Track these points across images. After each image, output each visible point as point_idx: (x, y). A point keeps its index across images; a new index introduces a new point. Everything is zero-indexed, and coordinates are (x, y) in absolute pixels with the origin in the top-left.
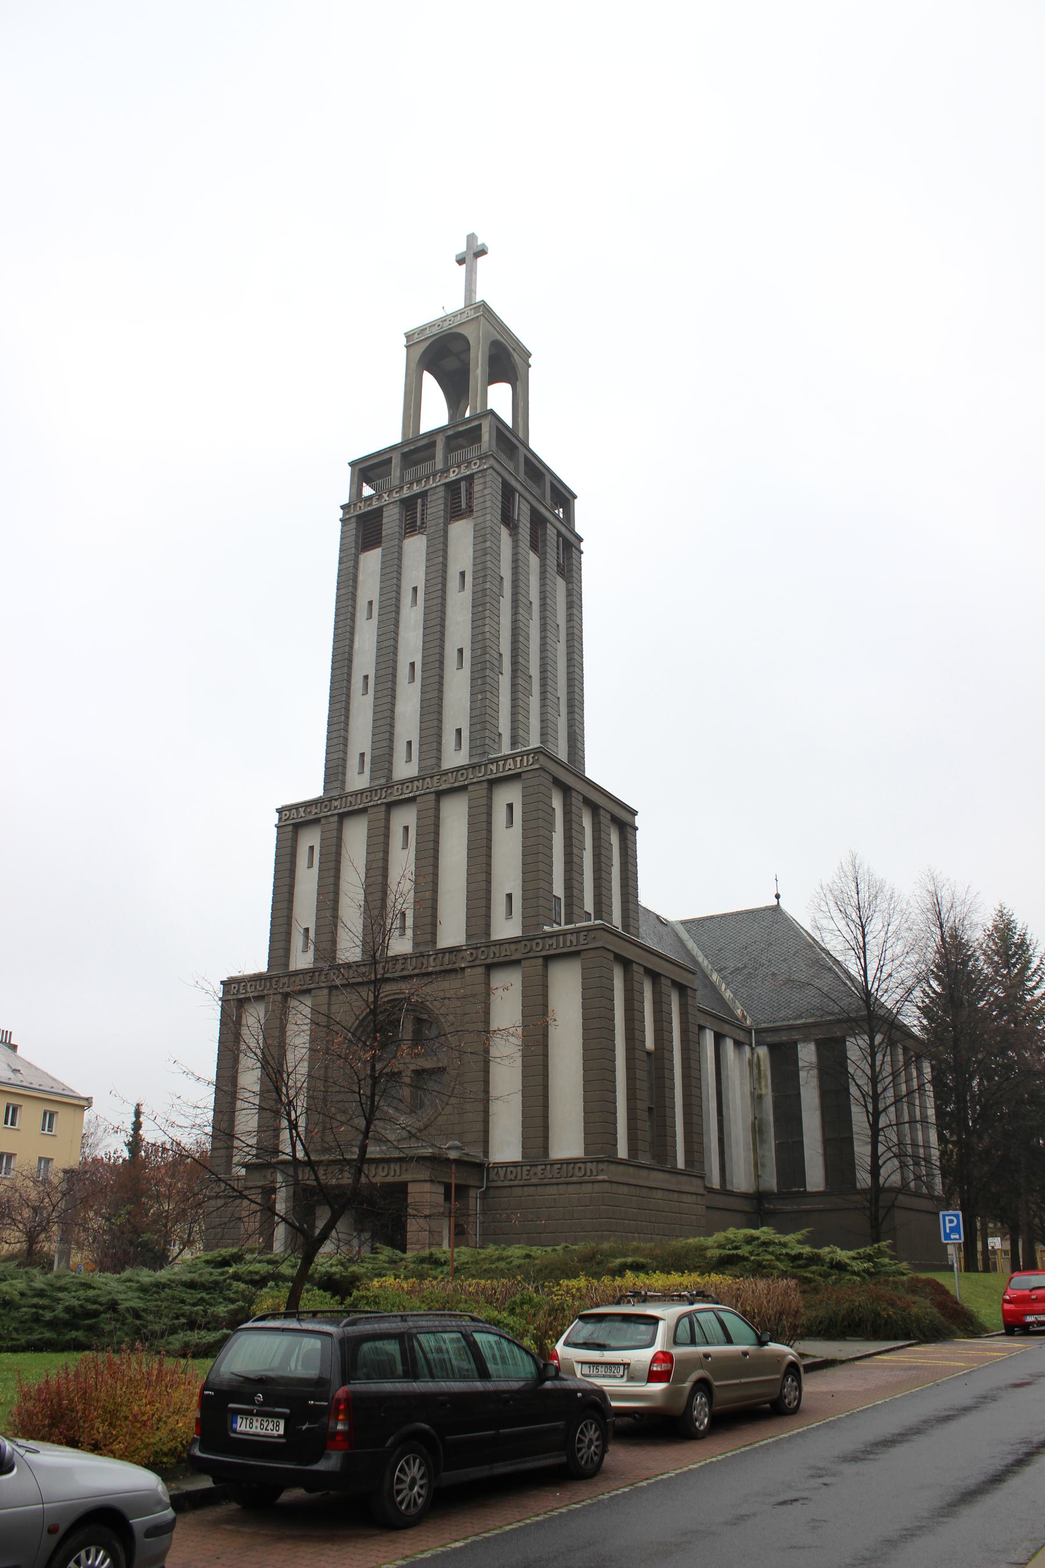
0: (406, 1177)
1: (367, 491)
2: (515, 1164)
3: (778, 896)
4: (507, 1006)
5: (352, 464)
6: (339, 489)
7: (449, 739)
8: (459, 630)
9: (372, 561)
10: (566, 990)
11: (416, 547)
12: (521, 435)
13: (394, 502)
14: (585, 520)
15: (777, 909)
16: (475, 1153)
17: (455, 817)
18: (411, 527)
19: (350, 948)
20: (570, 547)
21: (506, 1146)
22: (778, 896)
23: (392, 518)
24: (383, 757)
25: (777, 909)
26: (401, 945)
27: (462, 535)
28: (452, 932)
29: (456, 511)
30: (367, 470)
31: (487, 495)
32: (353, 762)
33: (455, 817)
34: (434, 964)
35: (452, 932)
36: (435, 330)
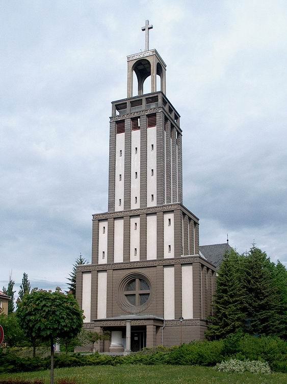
0: (145, 324)
1: (118, 113)
2: (173, 320)
3: (228, 240)
4: (169, 273)
5: (112, 103)
6: (109, 111)
7: (149, 197)
8: (152, 163)
9: (121, 137)
10: (187, 273)
11: (136, 135)
12: (164, 93)
13: (127, 116)
14: (183, 123)
15: (227, 244)
16: (162, 319)
17: (152, 221)
18: (136, 127)
19: (119, 258)
20: (179, 133)
21: (169, 314)
22: (228, 240)
23: (128, 124)
24: (127, 202)
25: (227, 244)
26: (135, 258)
27: (152, 132)
28: (152, 255)
29: (152, 124)
30: (119, 105)
31: (160, 119)
32: (117, 202)
33: (152, 221)
34: (145, 264)
35: (152, 255)
36: (138, 57)
